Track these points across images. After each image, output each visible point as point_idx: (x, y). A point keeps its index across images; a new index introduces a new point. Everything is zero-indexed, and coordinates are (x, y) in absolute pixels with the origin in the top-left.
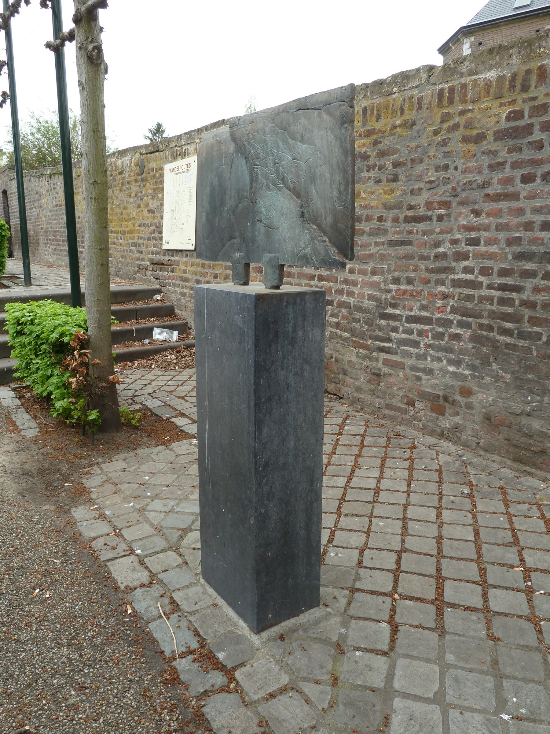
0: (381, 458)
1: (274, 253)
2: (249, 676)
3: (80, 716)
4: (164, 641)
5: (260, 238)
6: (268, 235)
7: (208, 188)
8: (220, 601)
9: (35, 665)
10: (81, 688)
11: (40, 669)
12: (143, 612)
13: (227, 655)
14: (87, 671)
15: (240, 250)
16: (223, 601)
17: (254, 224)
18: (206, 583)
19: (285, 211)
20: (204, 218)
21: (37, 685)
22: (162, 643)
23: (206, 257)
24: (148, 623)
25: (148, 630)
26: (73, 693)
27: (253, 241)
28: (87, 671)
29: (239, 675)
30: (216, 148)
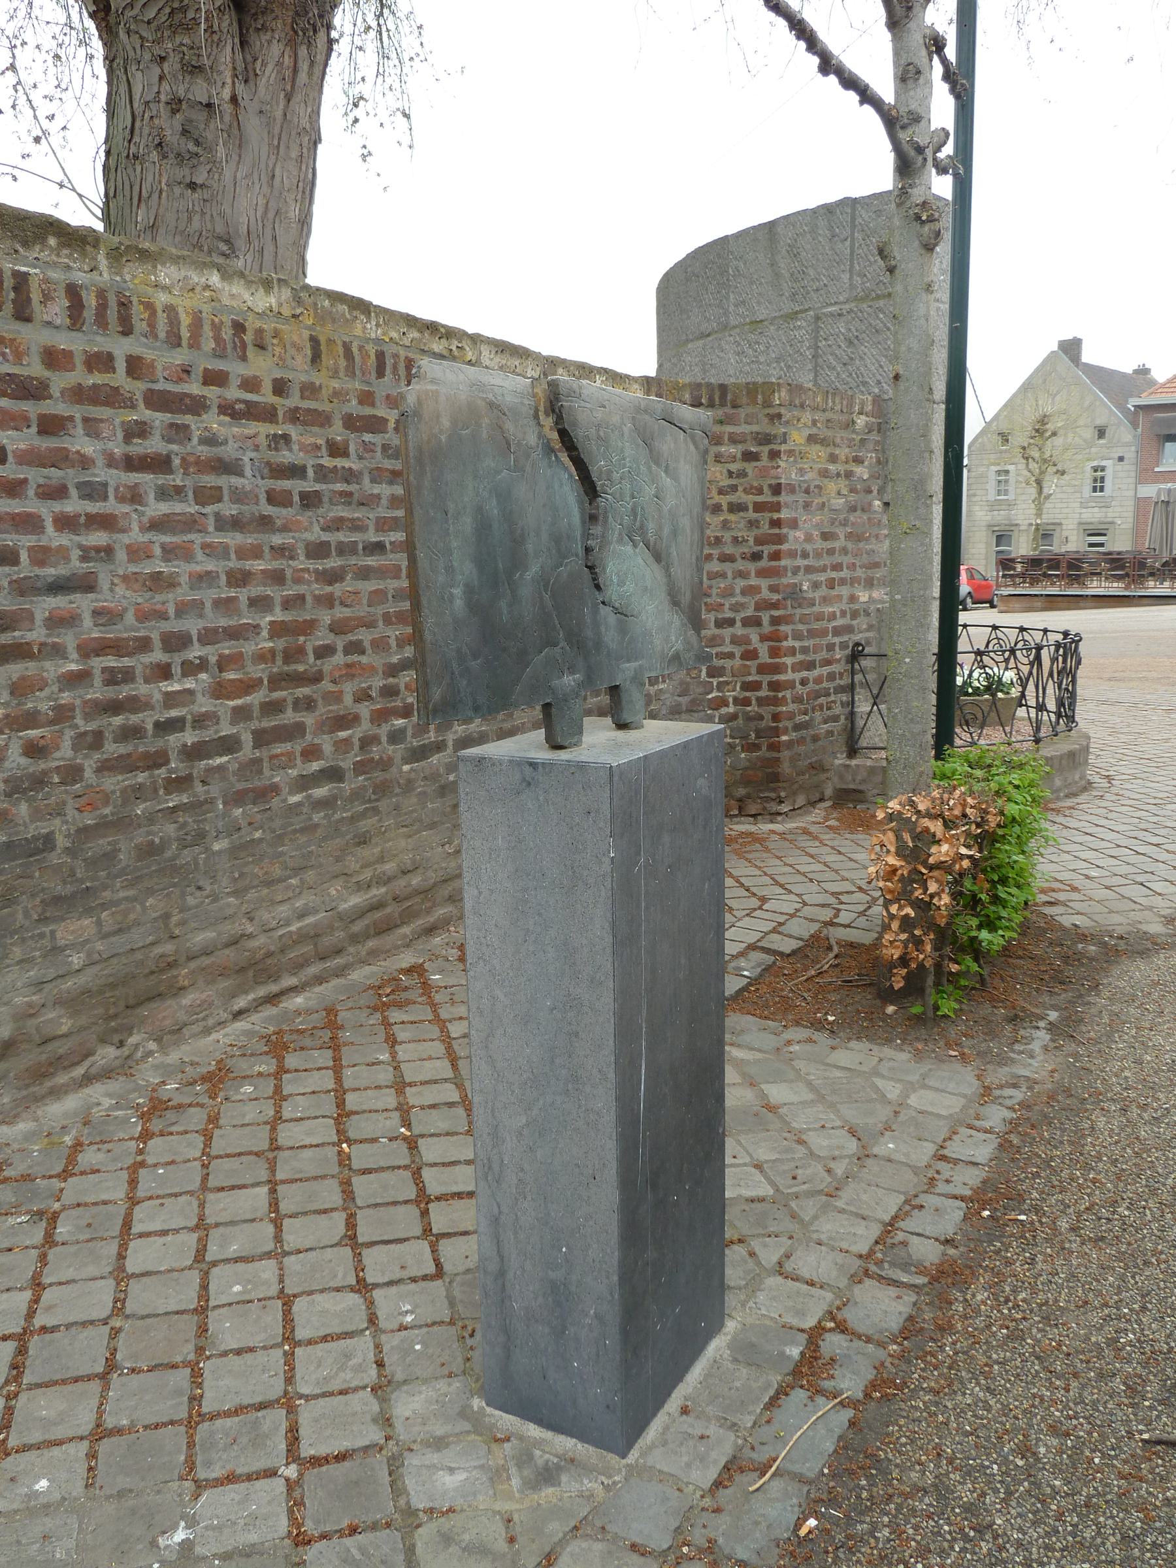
0: (128, 1168)
1: (636, 659)
2: (800, 1313)
3: (1057, 1414)
4: (831, 1431)
5: (610, 637)
6: (623, 630)
7: (469, 520)
8: (673, 1404)
9: (1070, 1534)
10: (1025, 1450)
11: (1068, 1519)
12: (795, 1501)
13: (786, 1345)
14: (995, 1467)
15: (572, 670)
16: (673, 1395)
17: (595, 608)
18: (637, 1446)
19: (649, 584)
20: (459, 603)
21: (1089, 1497)
22: (838, 1432)
23: (477, 709)
24: (810, 1482)
25: (826, 1471)
26: (1042, 1450)
27: (598, 644)
28: (995, 1467)
29: (810, 1322)
30: (486, 420)
